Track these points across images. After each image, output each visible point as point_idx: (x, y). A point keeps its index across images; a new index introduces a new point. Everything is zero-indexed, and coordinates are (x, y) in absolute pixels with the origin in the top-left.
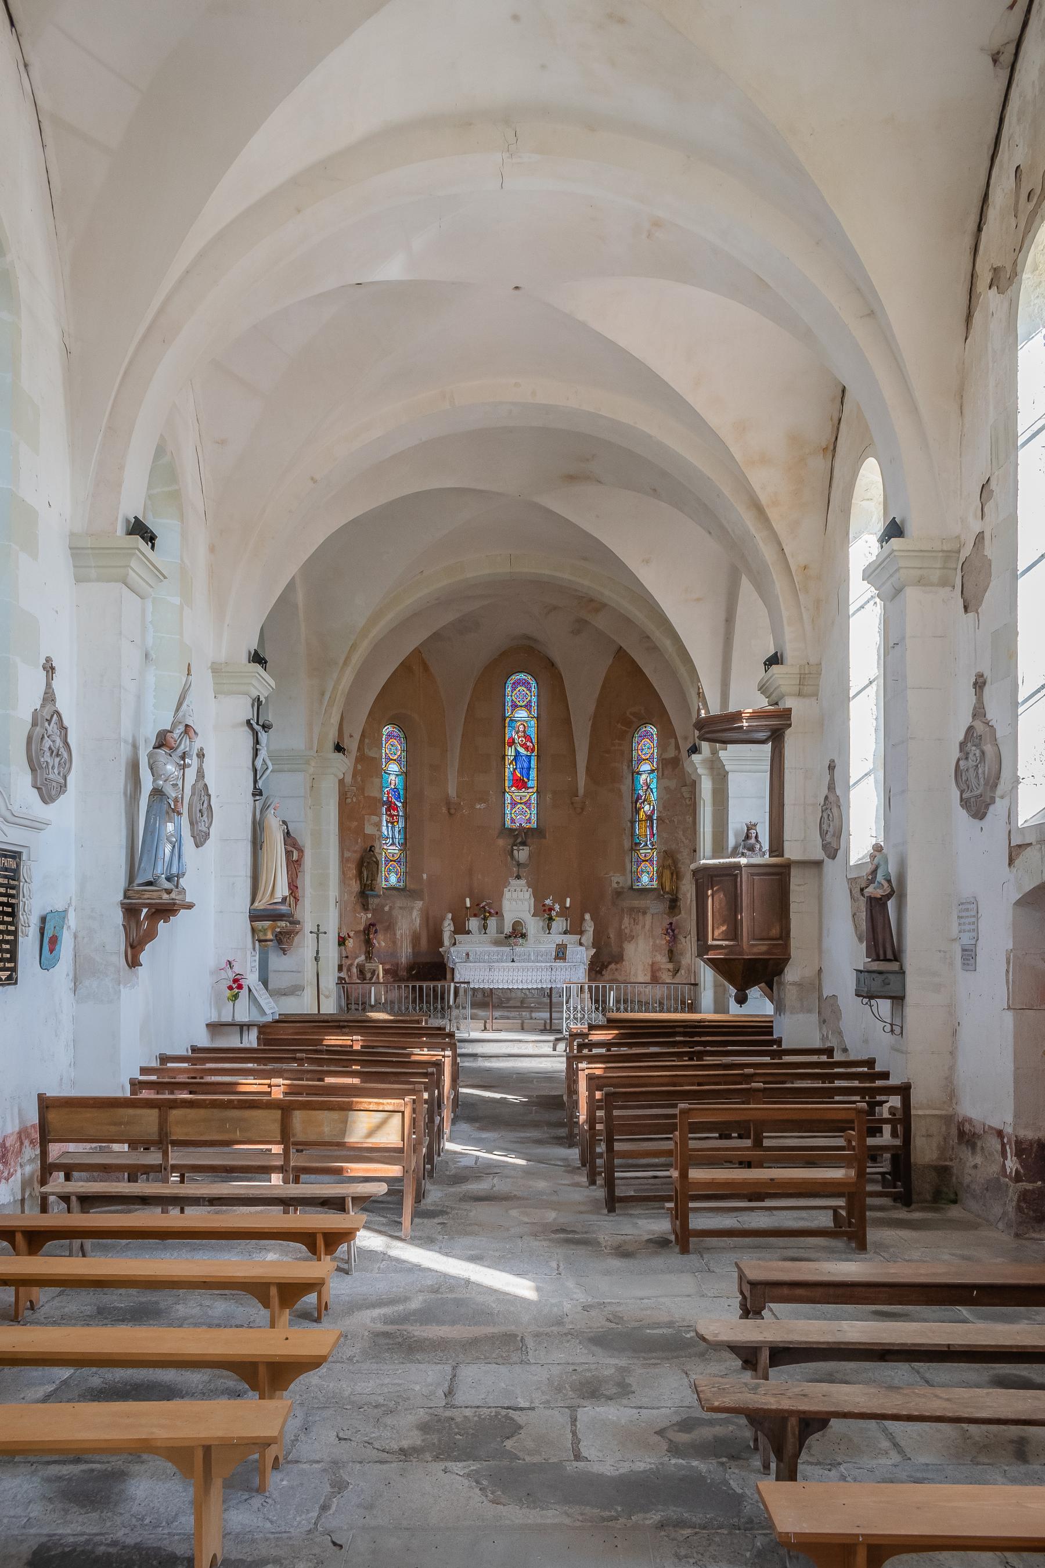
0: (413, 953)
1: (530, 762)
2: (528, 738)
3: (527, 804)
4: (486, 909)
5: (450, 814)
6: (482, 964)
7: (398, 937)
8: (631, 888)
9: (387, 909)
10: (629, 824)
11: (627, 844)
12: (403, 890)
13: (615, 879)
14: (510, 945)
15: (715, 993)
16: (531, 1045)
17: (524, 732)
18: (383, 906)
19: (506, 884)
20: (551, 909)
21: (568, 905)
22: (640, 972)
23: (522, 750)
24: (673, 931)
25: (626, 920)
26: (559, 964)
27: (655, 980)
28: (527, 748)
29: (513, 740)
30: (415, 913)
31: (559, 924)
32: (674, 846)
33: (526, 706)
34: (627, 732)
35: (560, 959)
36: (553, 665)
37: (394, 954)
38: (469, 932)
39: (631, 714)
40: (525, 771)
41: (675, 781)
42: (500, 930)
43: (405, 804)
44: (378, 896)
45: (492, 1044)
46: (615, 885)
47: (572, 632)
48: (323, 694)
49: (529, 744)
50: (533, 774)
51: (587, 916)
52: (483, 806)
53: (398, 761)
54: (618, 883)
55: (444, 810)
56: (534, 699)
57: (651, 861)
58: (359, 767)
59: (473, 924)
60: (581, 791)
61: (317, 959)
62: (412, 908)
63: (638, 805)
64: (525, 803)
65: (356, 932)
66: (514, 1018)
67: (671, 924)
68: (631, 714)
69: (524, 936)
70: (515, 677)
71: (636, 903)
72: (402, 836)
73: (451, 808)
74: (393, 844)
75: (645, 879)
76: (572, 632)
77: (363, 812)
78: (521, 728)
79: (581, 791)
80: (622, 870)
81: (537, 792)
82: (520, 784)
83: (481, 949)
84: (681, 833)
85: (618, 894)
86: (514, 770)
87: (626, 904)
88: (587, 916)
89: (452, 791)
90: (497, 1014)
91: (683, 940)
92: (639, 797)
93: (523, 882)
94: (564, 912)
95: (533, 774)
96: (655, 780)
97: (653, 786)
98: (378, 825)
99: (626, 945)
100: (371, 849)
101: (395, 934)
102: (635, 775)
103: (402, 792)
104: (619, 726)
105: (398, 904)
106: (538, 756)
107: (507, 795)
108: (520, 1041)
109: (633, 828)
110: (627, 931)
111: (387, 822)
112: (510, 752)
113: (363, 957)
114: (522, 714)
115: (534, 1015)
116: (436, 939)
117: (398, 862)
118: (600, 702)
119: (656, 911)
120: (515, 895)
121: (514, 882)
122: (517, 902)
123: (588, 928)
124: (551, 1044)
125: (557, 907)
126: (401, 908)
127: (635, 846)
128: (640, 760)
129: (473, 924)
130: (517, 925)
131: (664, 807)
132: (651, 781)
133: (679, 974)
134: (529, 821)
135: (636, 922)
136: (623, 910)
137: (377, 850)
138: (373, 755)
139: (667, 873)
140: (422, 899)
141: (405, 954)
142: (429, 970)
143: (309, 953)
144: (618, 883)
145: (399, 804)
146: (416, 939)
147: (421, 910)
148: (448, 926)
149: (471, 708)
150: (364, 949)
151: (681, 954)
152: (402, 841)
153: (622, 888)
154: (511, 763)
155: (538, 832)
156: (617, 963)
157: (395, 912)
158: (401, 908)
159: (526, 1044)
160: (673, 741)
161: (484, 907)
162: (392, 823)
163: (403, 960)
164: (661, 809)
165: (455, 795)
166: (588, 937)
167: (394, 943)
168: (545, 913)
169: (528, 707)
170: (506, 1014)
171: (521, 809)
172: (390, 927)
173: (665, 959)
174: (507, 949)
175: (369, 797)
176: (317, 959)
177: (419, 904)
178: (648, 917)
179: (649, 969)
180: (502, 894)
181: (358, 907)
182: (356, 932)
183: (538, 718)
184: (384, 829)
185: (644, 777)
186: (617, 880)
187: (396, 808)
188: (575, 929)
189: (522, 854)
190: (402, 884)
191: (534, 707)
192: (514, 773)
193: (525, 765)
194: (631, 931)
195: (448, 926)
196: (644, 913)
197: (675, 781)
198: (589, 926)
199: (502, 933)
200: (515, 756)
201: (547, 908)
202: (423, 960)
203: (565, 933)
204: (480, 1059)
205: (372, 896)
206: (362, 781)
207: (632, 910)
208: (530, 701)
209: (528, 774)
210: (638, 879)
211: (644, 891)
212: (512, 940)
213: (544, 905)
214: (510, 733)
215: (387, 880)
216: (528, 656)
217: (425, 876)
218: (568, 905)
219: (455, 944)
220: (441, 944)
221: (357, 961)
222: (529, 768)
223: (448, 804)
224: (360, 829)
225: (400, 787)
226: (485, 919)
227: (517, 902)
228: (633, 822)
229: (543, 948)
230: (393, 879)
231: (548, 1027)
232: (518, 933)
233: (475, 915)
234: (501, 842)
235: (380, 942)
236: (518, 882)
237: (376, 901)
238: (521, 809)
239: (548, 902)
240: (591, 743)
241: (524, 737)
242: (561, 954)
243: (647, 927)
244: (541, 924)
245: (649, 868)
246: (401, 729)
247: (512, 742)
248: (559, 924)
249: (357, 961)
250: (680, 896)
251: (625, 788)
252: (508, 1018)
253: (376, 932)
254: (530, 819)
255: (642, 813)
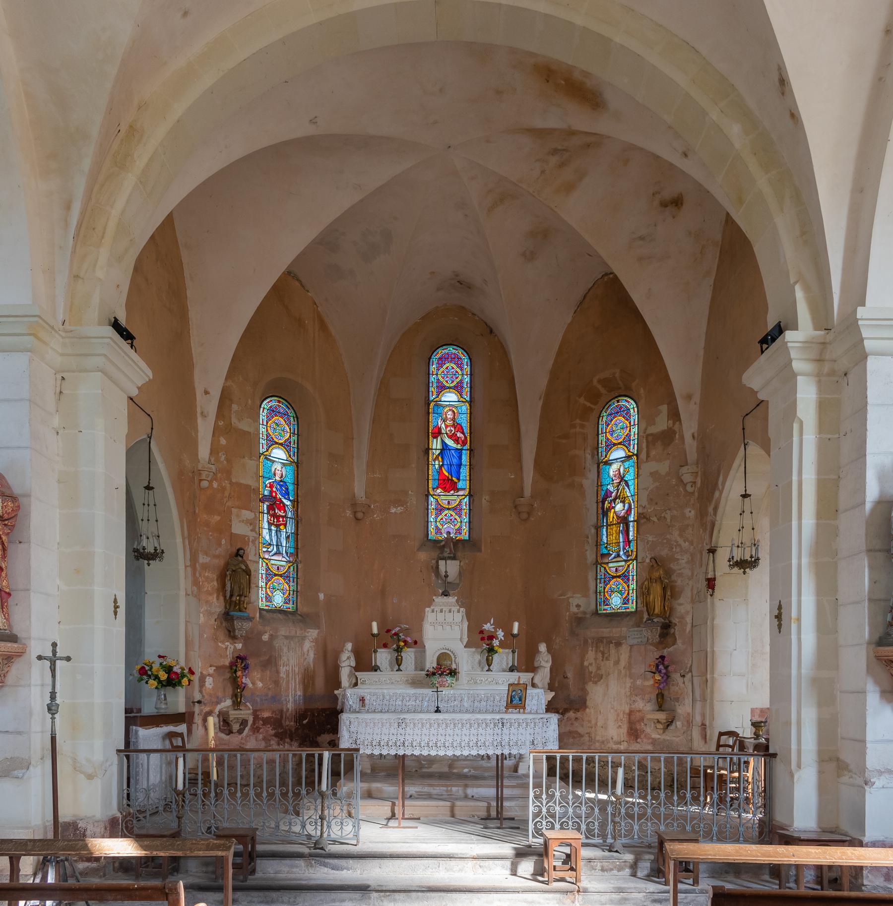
0: (304, 695)
1: (460, 458)
2: (458, 427)
3: (457, 509)
4: (400, 638)
5: (357, 519)
6: (385, 716)
7: (282, 675)
8: (596, 613)
9: (265, 637)
10: (593, 531)
11: (590, 556)
12: (293, 613)
13: (574, 601)
14: (433, 685)
15: (821, 772)
16: (471, 863)
17: (454, 419)
18: (261, 634)
19: (430, 603)
20: (491, 637)
21: (515, 631)
22: (611, 724)
23: (450, 443)
24: (666, 668)
25: (591, 655)
26: (513, 716)
27: (634, 733)
28: (457, 440)
29: (440, 429)
30: (307, 645)
31: (503, 658)
32: (665, 552)
33: (455, 388)
34: (592, 410)
35: (515, 707)
36: (491, 331)
37: (275, 698)
38: (376, 669)
39: (599, 381)
40: (454, 469)
41: (667, 463)
42: (420, 666)
43: (296, 503)
44: (249, 619)
45: (397, 862)
46: (574, 609)
47: (524, 254)
48: (68, 207)
49: (459, 434)
50: (465, 472)
51: (543, 647)
52: (399, 509)
53: (286, 446)
54: (578, 606)
55: (349, 513)
56: (467, 379)
57: (625, 577)
58: (223, 441)
59: (383, 657)
60: (528, 492)
61: (52, 709)
62: (303, 638)
63: (606, 505)
64: (454, 509)
65: (219, 668)
66: (439, 798)
67: (662, 657)
68: (599, 381)
69: (453, 673)
70: (441, 352)
71: (605, 632)
72: (292, 544)
73: (359, 512)
74: (278, 553)
75: (616, 601)
76: (524, 254)
77: (229, 504)
78: (450, 415)
79: (528, 492)
80: (584, 590)
81: (470, 495)
82: (448, 485)
83: (391, 692)
84: (676, 533)
85: (579, 620)
86: (441, 467)
87: (592, 632)
88: (543, 647)
89: (359, 490)
90: (411, 789)
91: (680, 680)
92: (608, 494)
93: (452, 600)
94: (510, 641)
95: (465, 472)
96: (632, 470)
97: (630, 477)
98: (255, 525)
99: (590, 687)
100: (239, 554)
101: (278, 672)
102: (602, 466)
103: (291, 488)
104: (582, 400)
105: (283, 631)
106: (471, 450)
107: (431, 499)
108: (450, 857)
109: (598, 535)
110: (592, 669)
111: (270, 524)
112: (436, 444)
113: (228, 702)
114: (450, 397)
115: (470, 791)
116: (334, 681)
117: (285, 576)
118: (554, 376)
119: (635, 642)
120: (441, 617)
121: (439, 600)
122: (444, 628)
123: (543, 664)
124: (508, 863)
125: (500, 634)
126: (286, 637)
127: (601, 558)
128: (610, 446)
129: (383, 657)
130: (443, 657)
131: (650, 500)
132: (627, 470)
133: (672, 727)
134: (459, 531)
135: (605, 657)
136: (586, 642)
137: (251, 556)
138: (246, 429)
139: (657, 589)
140: (318, 627)
141: (292, 697)
142: (318, 722)
143: (38, 698)
144: (578, 606)
145: (287, 503)
146: (308, 679)
147: (316, 641)
148: (347, 661)
149: (384, 385)
150: (230, 690)
151: (677, 700)
152: (292, 550)
153: (585, 613)
154: (437, 458)
155: (472, 544)
156: (577, 710)
157: (277, 643)
158: (286, 637)
159: (461, 863)
160: (664, 408)
161: (396, 634)
162: (277, 526)
163: (290, 706)
164: (644, 502)
165: (363, 494)
166: (543, 676)
167: (277, 683)
168: (483, 642)
169: (458, 388)
170: (426, 789)
171: (449, 517)
172: (270, 662)
173: (649, 707)
174: (428, 692)
175: (239, 485)
176: (52, 709)
177: (313, 633)
178: (624, 651)
179: (625, 720)
180: (421, 618)
181: (221, 635)
182: (219, 668)
183: (471, 402)
184: (265, 532)
185: (615, 467)
186: (577, 602)
187: (283, 507)
188: (528, 664)
189: (451, 568)
190: (290, 606)
191: (467, 390)
192: (440, 472)
193: (455, 461)
194: (598, 668)
195: (347, 661)
196: (618, 644)
197: (667, 463)
198: (545, 660)
199: (422, 670)
200: (442, 450)
201: (485, 635)
202: (319, 705)
203: (511, 670)
204: (374, 895)
205: (241, 618)
206: (227, 460)
207: (599, 640)
208: (461, 382)
209: (458, 473)
210: (606, 602)
211: (616, 617)
212: (436, 679)
213: (482, 632)
214: (435, 421)
215: (268, 599)
216: (460, 322)
217: (321, 596)
218: (515, 631)
219: (356, 684)
220: (338, 685)
221: (218, 708)
222: (460, 465)
223: (354, 505)
224: (224, 528)
225: (290, 479)
226: (399, 650)
227: (444, 628)
228: (598, 528)
229: (483, 690)
230: (278, 600)
231: (494, 814)
232: (445, 670)
233: (385, 646)
234: (423, 556)
235: (254, 681)
236: (445, 599)
237: (247, 625)
238: (449, 517)
239: (488, 627)
240: (541, 429)
241: (453, 426)
242: (516, 700)
243: (623, 663)
244: (478, 657)
245: (622, 585)
246: (290, 405)
247: (438, 433)
248: (503, 658)
249: (218, 708)
250: (675, 620)
251: (588, 482)
252: (429, 797)
253: (246, 668)
254: (460, 529)
255: (611, 514)
